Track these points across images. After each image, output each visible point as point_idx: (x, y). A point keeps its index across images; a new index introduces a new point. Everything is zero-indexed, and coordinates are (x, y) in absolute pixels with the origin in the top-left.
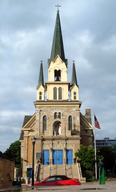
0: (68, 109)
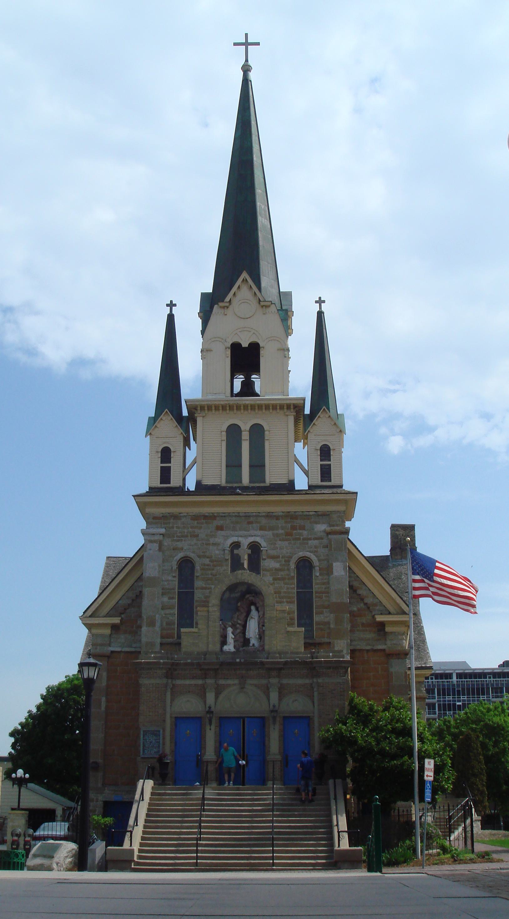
0: (294, 528)
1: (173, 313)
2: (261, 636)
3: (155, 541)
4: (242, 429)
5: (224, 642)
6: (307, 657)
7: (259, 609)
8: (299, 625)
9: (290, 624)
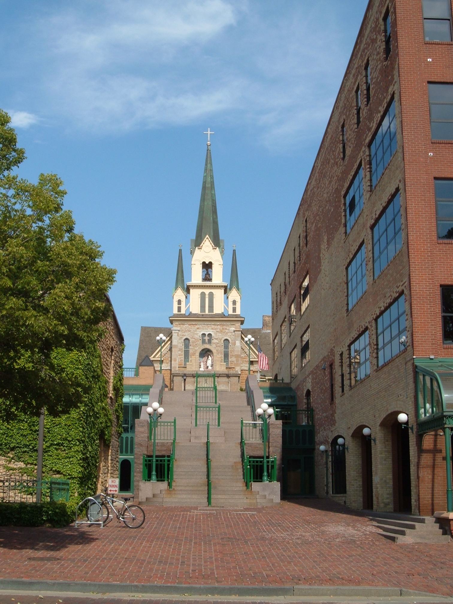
0: (223, 329)
2: (212, 366)
3: (176, 333)
5: (200, 367)
6: (227, 373)
8: (224, 362)
9: (221, 362)
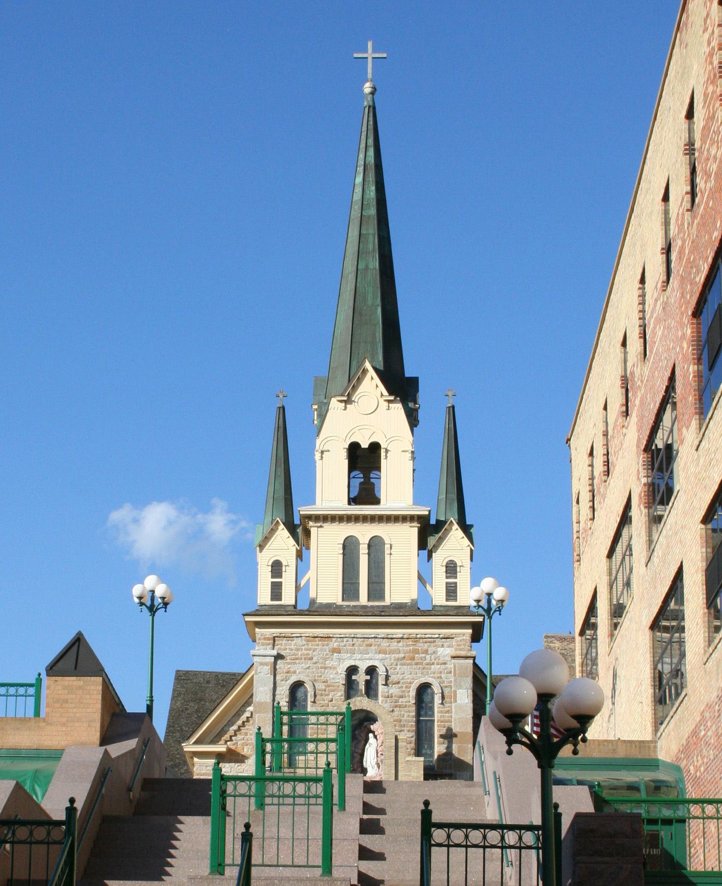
1: (539, 771)
4: (361, 542)
7: (378, 737)
